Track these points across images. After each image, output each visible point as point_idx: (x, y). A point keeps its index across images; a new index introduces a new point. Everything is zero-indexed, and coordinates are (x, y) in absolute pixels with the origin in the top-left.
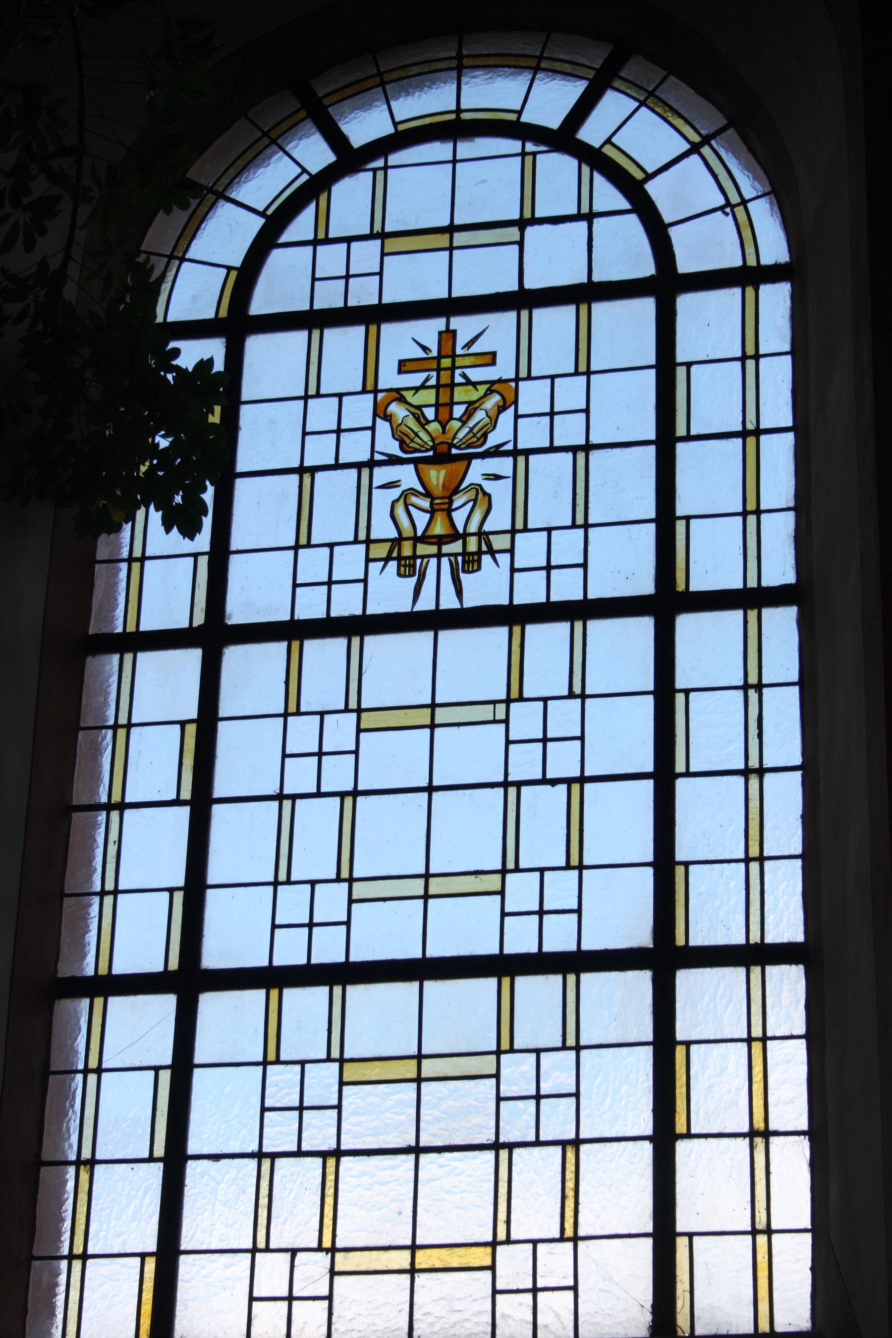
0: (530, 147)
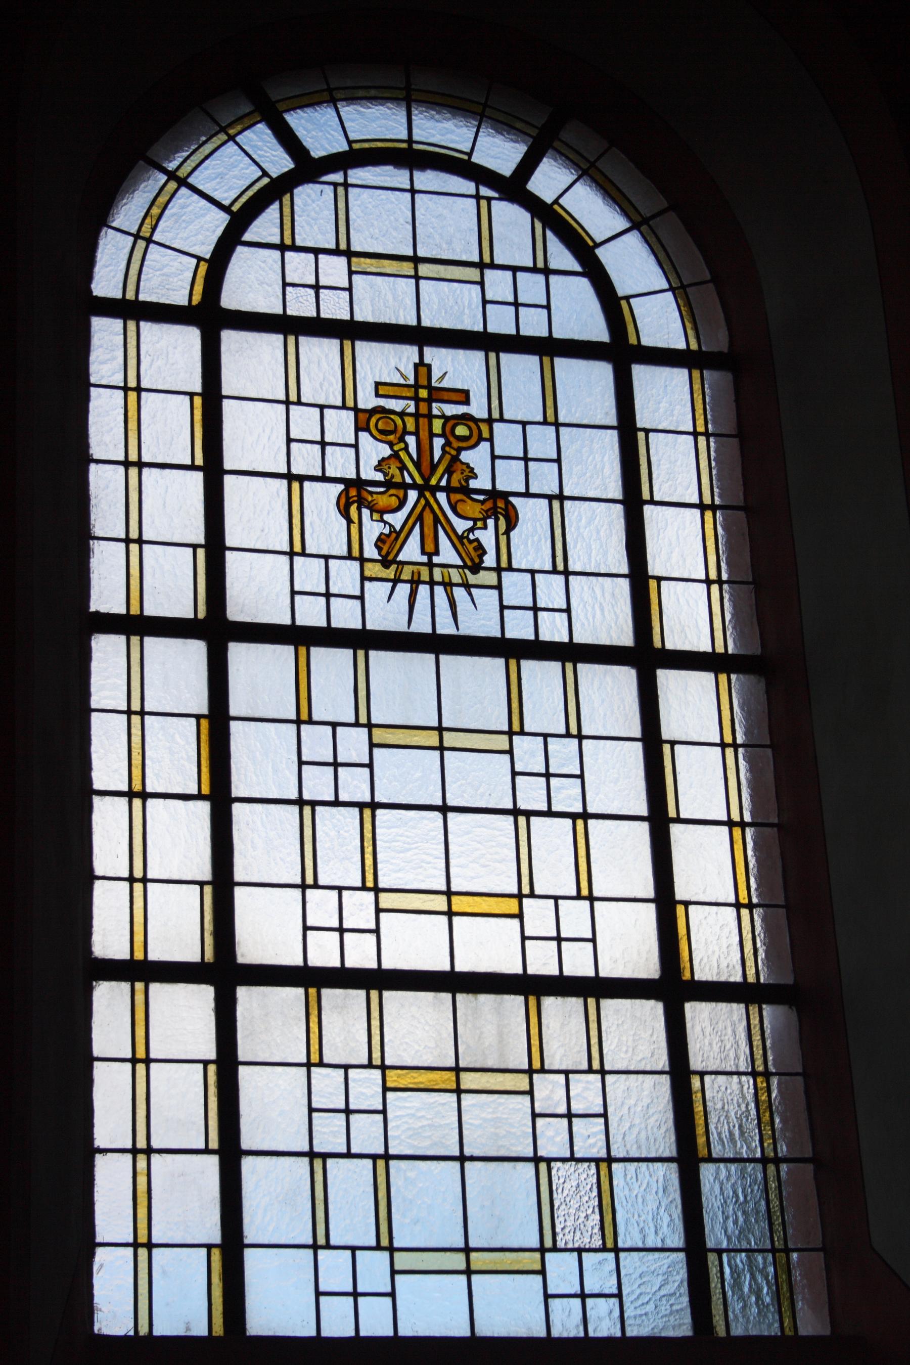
0: (485, 191)
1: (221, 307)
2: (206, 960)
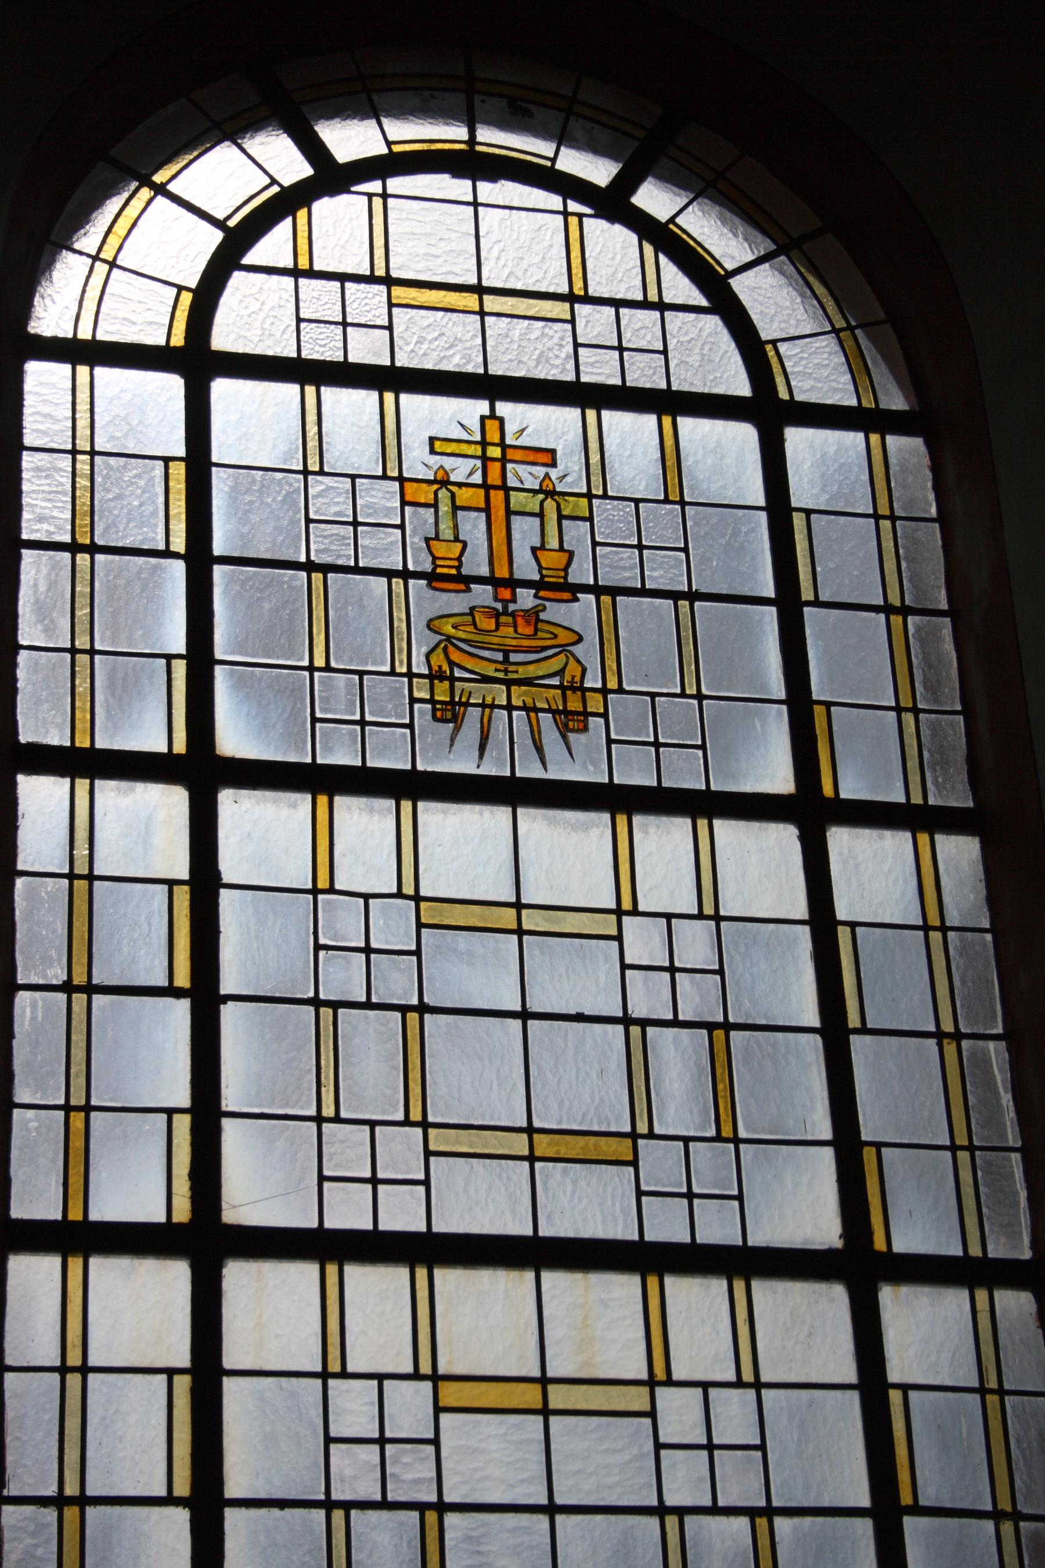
0: (573, 206)
2: (175, 751)
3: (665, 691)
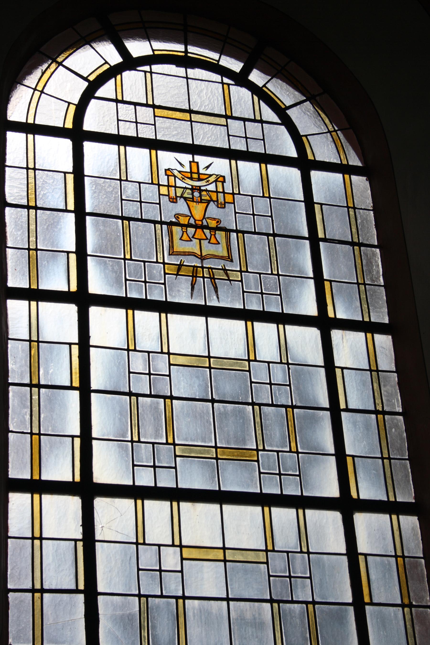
0: (226, 80)
1: (77, 305)
2: (71, 290)
3: (230, 269)
